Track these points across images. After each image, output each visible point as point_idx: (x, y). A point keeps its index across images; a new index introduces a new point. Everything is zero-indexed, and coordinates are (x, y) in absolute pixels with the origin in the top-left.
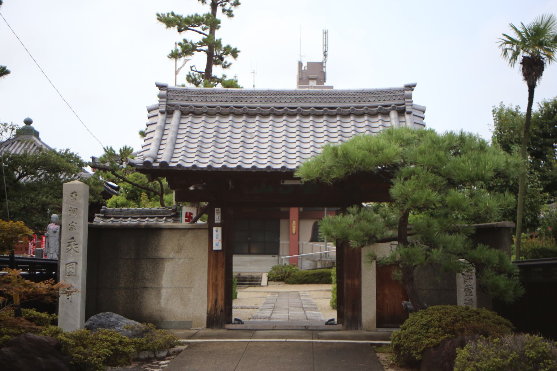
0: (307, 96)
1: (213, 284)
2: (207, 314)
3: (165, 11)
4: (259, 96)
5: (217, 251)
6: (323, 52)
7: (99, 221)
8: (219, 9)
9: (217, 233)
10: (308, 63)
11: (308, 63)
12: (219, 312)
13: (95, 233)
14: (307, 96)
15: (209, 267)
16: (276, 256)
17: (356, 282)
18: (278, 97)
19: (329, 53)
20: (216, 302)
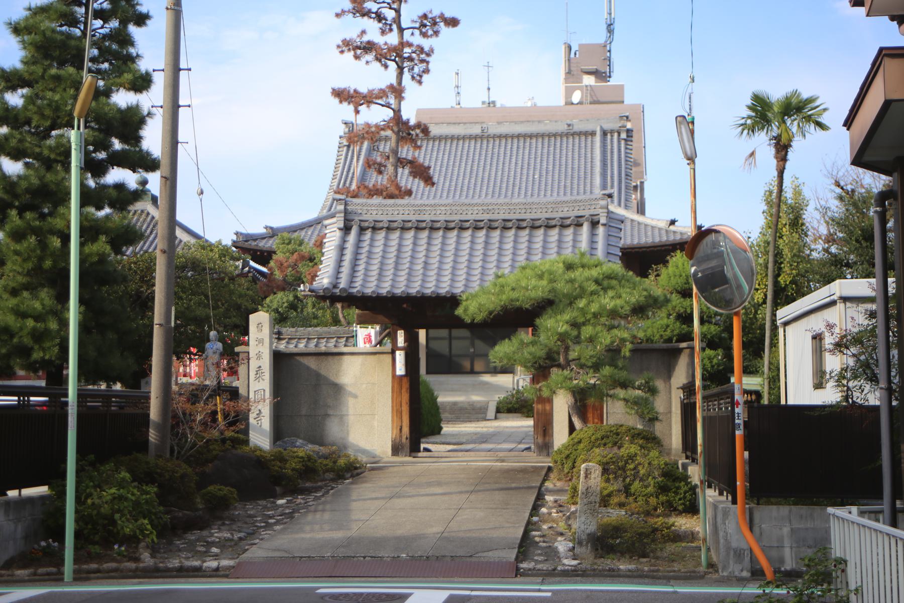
0: (496, 207)
1: (397, 411)
2: (252, 249)
3: (341, 85)
4: (443, 208)
5: (401, 376)
6: (605, 26)
7: (282, 346)
8: (407, 76)
9: (400, 356)
10: (580, 45)
11: (580, 45)
12: (404, 440)
13: (278, 358)
14: (496, 207)
15: (393, 392)
16: (511, 375)
17: (548, 408)
18: (464, 208)
19: (617, 27)
20: (401, 429)
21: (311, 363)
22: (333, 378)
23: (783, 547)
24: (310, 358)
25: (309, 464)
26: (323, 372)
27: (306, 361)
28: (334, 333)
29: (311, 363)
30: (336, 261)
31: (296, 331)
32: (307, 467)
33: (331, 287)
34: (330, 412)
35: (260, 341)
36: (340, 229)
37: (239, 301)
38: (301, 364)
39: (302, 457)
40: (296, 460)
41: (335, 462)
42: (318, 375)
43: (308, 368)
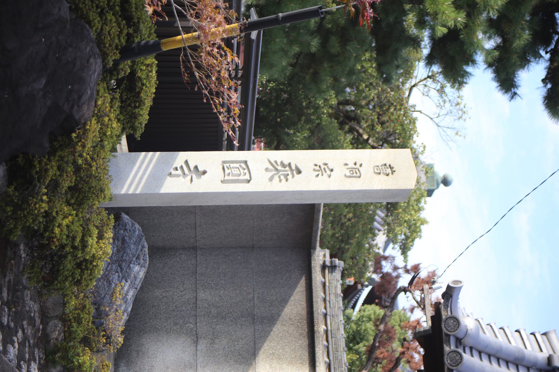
21: (295, 305)
22: (267, 347)
23: (253, 323)
24: (304, 304)
25: (69, 264)
26: (278, 329)
27: (298, 296)
28: (336, 358)
29: (295, 305)
30: (500, 350)
31: (336, 295)
32: (59, 257)
33: (460, 333)
34: (202, 345)
35: (355, 172)
36: (550, 359)
37: (353, 241)
38: (293, 287)
39: (84, 245)
40: (77, 228)
41: (86, 342)
42: (271, 320)
43: (284, 301)
